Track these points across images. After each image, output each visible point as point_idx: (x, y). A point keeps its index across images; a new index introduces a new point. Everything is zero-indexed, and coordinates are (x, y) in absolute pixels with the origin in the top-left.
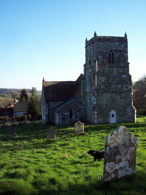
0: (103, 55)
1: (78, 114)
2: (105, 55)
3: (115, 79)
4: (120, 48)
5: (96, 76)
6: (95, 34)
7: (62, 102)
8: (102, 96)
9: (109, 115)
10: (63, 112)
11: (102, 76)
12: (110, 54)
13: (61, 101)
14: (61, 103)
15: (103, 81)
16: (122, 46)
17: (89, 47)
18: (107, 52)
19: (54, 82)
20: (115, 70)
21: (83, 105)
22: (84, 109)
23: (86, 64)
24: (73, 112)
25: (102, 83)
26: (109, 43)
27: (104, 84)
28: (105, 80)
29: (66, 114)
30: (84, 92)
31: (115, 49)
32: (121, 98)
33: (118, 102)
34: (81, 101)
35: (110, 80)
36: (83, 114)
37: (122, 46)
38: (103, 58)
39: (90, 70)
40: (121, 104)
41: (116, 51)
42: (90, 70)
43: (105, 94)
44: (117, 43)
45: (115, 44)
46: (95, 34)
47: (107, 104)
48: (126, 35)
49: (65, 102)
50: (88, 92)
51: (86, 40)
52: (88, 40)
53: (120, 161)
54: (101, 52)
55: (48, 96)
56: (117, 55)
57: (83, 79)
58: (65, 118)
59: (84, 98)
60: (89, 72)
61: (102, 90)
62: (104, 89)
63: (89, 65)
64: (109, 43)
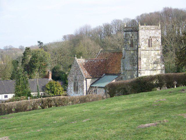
11: (144, 58)
14: (96, 79)
15: (145, 62)
16: (157, 33)
20: (153, 52)
25: (144, 63)
26: (148, 32)
27: (146, 63)
28: (146, 61)
35: (150, 61)
37: (157, 33)
39: (132, 52)
44: (154, 31)
54: (143, 38)
57: (123, 59)
59: (124, 74)
62: (145, 68)
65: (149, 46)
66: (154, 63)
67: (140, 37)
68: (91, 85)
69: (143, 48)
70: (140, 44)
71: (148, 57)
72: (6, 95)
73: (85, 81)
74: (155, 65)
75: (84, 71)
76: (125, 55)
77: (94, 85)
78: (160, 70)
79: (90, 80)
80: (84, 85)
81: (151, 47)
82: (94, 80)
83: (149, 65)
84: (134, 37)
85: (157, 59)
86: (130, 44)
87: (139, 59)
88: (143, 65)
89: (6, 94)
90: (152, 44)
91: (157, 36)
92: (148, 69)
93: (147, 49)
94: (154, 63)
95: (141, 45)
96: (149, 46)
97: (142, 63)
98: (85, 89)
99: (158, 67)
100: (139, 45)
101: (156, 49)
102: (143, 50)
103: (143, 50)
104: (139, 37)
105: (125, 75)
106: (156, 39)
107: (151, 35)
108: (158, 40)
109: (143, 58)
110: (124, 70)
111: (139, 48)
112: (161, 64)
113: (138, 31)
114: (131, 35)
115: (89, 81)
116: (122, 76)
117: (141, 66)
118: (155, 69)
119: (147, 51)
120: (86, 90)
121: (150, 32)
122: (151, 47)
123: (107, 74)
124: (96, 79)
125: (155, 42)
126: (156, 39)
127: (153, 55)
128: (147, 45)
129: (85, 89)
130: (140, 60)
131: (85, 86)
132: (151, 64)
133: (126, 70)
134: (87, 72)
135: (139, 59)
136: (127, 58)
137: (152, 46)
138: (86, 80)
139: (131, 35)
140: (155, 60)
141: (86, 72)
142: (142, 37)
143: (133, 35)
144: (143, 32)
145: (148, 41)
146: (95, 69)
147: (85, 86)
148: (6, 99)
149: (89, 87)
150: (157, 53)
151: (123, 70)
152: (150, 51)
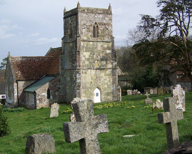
0: (87, 28)
1: (57, 94)
2: (89, 28)
3: (99, 54)
4: (104, 21)
5: (176, 45)
6: (78, 4)
7: (34, 82)
8: (86, 73)
9: (92, 94)
10: (40, 91)
11: (86, 51)
12: (94, 27)
13: (32, 80)
14: (33, 82)
15: (87, 57)
16: (106, 18)
17: (69, 18)
18: (91, 25)
19: (26, 57)
20: (99, 44)
21: (62, 84)
22: (63, 88)
23: (65, 37)
24: (50, 92)
25: (86, 59)
26: (93, 15)
27: (88, 59)
28: (89, 56)
29: (43, 94)
30: (63, 69)
31: (99, 22)
32: (105, 75)
33: (102, 79)
34: (60, 80)
35: (95, 56)
36: (61, 94)
37: (106, 18)
38: (87, 31)
39: (71, 44)
40: (106, 82)
41: (101, 24)
42: (71, 44)
43: (89, 70)
44: (101, 16)
45: (99, 16)
46: (78, 4)
47: (91, 82)
48: (110, 7)
49: (37, 81)
50: (68, 70)
51: (65, 9)
52: (67, 10)
53: (179, 103)
54: (84, 24)
55: (17, 74)
56: (101, 28)
57: (62, 54)
58: (42, 100)
59: (62, 75)
60: (70, 47)
61: (86, 66)
62: (88, 65)
63: (70, 38)
64: (93, 15)
65: (94, 36)
66: (102, 60)
67: (79, 23)
68: (24, 89)
69: (85, 38)
70: (79, 32)
71: (92, 51)
72: (3, 95)
73: (15, 84)
74: (104, 63)
75: (17, 71)
76: (64, 50)
77: (26, 90)
78: (111, 70)
79: (24, 82)
80: (14, 90)
81: (98, 37)
82: (29, 83)
83: (94, 62)
84: (74, 24)
85: (106, 54)
86: (70, 34)
87: (77, 53)
88: (84, 62)
89: (3, 94)
90: (98, 33)
91: (106, 22)
92: (92, 68)
93: (91, 39)
94: (102, 60)
95: (82, 33)
96: (94, 36)
97: (83, 59)
98: (16, 94)
99: (108, 65)
100: (78, 33)
101: (104, 41)
102: (84, 41)
103: (84, 41)
104: (78, 22)
105: (65, 76)
106: (104, 27)
107: (98, 21)
108: (107, 27)
109: (84, 52)
110: (63, 69)
111: (77, 38)
112: (113, 61)
113: (77, 15)
114: (70, 22)
115: (21, 84)
116: (60, 77)
117: (79, 63)
118: (102, 67)
119: (91, 43)
120: (18, 96)
121: (96, 17)
122: (98, 37)
123: (47, 76)
124: (33, 82)
125: (103, 31)
126: (104, 27)
127: (99, 48)
128: (91, 34)
129: (16, 94)
130: (79, 54)
131: (16, 90)
132: (96, 61)
133: (66, 70)
134: (20, 73)
135: (77, 53)
136: (67, 54)
137: (98, 35)
138: (17, 83)
139: (70, 22)
140: (104, 55)
141: (19, 72)
142: (83, 22)
143: (72, 21)
144: (84, 15)
145: (92, 29)
146: (33, 69)
147: (16, 90)
148: (99, 94)
149: (21, 92)
150: (106, 46)
151: (61, 69)
152: (95, 43)
